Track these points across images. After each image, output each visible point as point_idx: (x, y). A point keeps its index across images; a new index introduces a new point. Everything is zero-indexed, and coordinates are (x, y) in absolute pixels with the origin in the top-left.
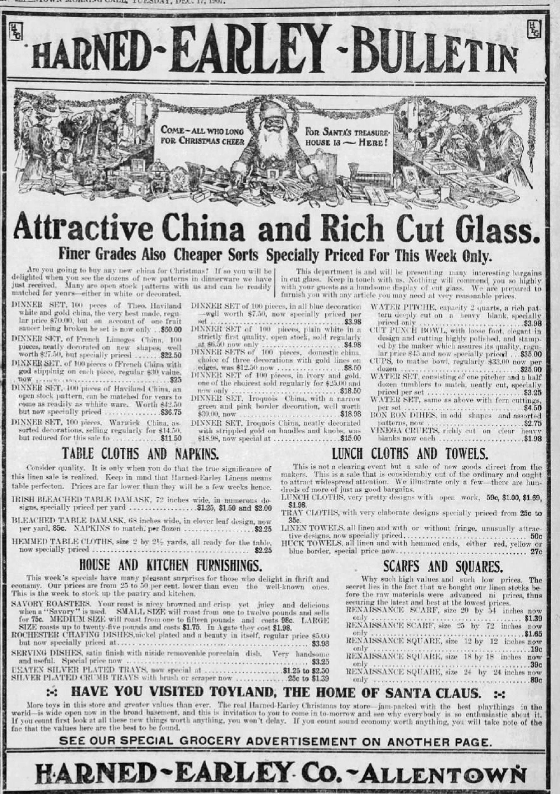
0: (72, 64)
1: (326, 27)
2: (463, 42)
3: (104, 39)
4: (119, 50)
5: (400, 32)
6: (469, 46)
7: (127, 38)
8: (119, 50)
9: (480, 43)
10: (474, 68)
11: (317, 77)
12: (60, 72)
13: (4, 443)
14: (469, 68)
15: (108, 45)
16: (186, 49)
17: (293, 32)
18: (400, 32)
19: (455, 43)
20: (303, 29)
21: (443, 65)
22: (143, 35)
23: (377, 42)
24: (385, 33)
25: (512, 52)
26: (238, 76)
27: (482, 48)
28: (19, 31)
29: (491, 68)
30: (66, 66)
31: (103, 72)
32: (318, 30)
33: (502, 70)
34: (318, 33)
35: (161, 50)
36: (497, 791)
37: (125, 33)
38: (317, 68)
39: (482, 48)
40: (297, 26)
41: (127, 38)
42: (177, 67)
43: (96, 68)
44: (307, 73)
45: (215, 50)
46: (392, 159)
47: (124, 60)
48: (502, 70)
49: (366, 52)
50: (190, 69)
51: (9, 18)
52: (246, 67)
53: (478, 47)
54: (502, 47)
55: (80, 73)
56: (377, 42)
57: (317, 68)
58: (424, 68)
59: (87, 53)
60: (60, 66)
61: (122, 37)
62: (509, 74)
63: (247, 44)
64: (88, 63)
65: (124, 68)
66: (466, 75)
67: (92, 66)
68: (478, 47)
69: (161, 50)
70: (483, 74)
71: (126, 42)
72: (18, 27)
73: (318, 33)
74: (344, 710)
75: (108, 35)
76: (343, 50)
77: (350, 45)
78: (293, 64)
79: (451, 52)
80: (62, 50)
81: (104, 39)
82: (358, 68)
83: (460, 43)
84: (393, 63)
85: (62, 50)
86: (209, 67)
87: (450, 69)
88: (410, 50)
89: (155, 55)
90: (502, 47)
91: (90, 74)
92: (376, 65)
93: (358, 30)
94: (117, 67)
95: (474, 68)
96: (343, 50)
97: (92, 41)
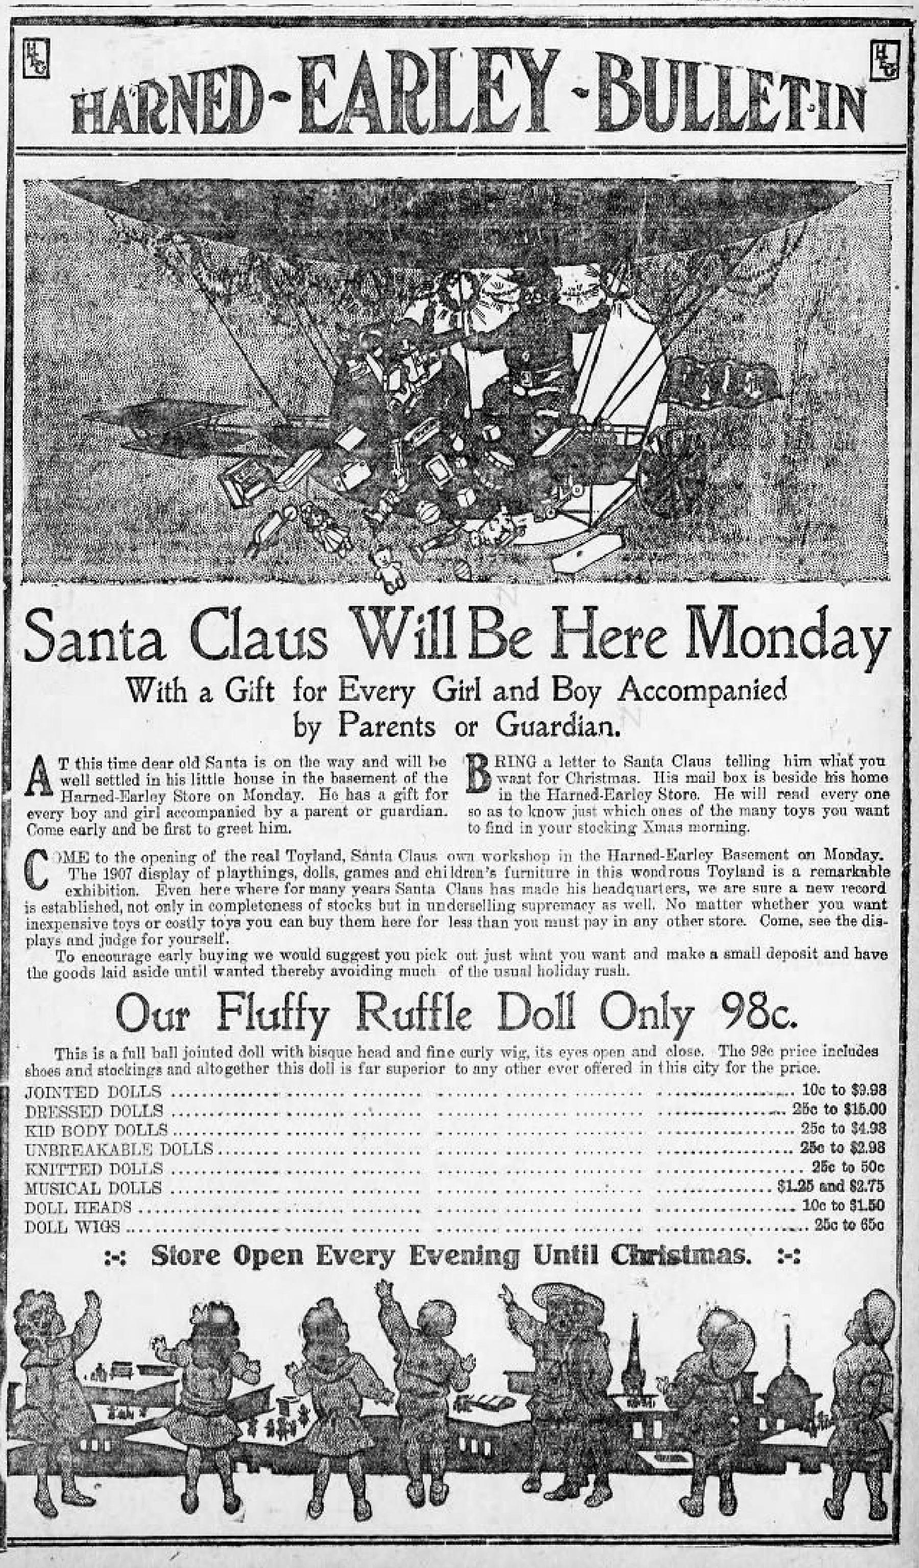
0: (135, 128)
1: (553, 54)
2: (777, 80)
3: (187, 82)
4: (213, 101)
5: (673, 64)
6: (787, 87)
7: (225, 80)
8: (213, 101)
9: (806, 82)
10: (795, 124)
11: (538, 139)
12: (118, 138)
13: (9, 692)
14: (787, 125)
15: (195, 95)
16: (322, 95)
17: (498, 63)
18: (673, 64)
19: (764, 83)
20: (515, 55)
21: (743, 118)
22: (251, 73)
23: (637, 81)
24: (650, 63)
25: (856, 96)
26: (409, 139)
27: (808, 89)
28: (42, 57)
29: (823, 124)
30: (128, 130)
31: (186, 137)
32: (540, 60)
33: (841, 126)
34: (540, 64)
35: (282, 97)
36: (4, 1354)
37: (222, 71)
38: (538, 124)
39: (808, 89)
40: (506, 52)
41: (225, 80)
42: (308, 126)
43: (175, 130)
44: (519, 135)
45: (370, 93)
46: (507, 1474)
47: (221, 116)
48: (841, 126)
49: (619, 96)
50: (327, 129)
51: (22, 31)
52: (422, 123)
53: (803, 89)
54: (842, 89)
55: (151, 139)
56: (637, 81)
57: (538, 124)
58: (715, 124)
59: (160, 106)
60: (118, 129)
61: (217, 77)
62: (851, 135)
63: (422, 84)
64: (163, 124)
65: (222, 130)
66: (781, 135)
67: (170, 128)
68: (803, 89)
69: (282, 97)
70: (810, 134)
71: (223, 85)
72: (41, 47)
73: (540, 64)
74: (720, 820)
75: (194, 75)
76: (582, 93)
77: (592, 85)
78: (497, 118)
79: (757, 97)
80: (120, 106)
81: (187, 82)
82: (606, 125)
83: (771, 82)
84: (662, 115)
85: (120, 106)
86: (360, 125)
87: (757, 126)
88: (692, 99)
89: (270, 107)
90: (842, 89)
91: (165, 140)
92: (635, 120)
93: (605, 58)
94: (208, 128)
95: (795, 124)
96: (582, 93)
97: (168, 86)
